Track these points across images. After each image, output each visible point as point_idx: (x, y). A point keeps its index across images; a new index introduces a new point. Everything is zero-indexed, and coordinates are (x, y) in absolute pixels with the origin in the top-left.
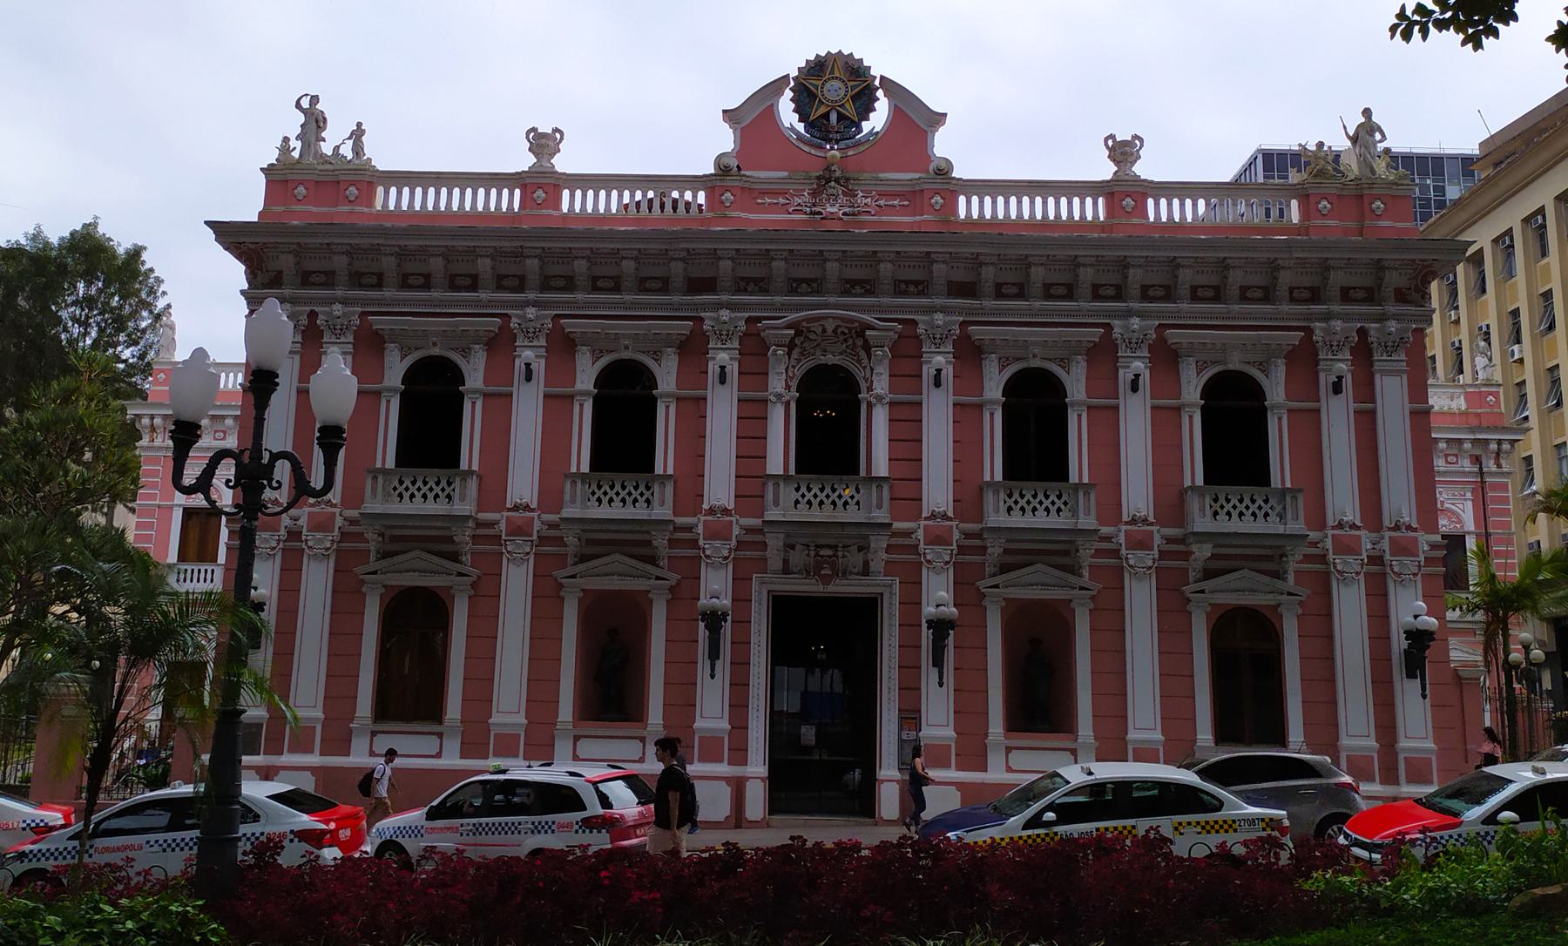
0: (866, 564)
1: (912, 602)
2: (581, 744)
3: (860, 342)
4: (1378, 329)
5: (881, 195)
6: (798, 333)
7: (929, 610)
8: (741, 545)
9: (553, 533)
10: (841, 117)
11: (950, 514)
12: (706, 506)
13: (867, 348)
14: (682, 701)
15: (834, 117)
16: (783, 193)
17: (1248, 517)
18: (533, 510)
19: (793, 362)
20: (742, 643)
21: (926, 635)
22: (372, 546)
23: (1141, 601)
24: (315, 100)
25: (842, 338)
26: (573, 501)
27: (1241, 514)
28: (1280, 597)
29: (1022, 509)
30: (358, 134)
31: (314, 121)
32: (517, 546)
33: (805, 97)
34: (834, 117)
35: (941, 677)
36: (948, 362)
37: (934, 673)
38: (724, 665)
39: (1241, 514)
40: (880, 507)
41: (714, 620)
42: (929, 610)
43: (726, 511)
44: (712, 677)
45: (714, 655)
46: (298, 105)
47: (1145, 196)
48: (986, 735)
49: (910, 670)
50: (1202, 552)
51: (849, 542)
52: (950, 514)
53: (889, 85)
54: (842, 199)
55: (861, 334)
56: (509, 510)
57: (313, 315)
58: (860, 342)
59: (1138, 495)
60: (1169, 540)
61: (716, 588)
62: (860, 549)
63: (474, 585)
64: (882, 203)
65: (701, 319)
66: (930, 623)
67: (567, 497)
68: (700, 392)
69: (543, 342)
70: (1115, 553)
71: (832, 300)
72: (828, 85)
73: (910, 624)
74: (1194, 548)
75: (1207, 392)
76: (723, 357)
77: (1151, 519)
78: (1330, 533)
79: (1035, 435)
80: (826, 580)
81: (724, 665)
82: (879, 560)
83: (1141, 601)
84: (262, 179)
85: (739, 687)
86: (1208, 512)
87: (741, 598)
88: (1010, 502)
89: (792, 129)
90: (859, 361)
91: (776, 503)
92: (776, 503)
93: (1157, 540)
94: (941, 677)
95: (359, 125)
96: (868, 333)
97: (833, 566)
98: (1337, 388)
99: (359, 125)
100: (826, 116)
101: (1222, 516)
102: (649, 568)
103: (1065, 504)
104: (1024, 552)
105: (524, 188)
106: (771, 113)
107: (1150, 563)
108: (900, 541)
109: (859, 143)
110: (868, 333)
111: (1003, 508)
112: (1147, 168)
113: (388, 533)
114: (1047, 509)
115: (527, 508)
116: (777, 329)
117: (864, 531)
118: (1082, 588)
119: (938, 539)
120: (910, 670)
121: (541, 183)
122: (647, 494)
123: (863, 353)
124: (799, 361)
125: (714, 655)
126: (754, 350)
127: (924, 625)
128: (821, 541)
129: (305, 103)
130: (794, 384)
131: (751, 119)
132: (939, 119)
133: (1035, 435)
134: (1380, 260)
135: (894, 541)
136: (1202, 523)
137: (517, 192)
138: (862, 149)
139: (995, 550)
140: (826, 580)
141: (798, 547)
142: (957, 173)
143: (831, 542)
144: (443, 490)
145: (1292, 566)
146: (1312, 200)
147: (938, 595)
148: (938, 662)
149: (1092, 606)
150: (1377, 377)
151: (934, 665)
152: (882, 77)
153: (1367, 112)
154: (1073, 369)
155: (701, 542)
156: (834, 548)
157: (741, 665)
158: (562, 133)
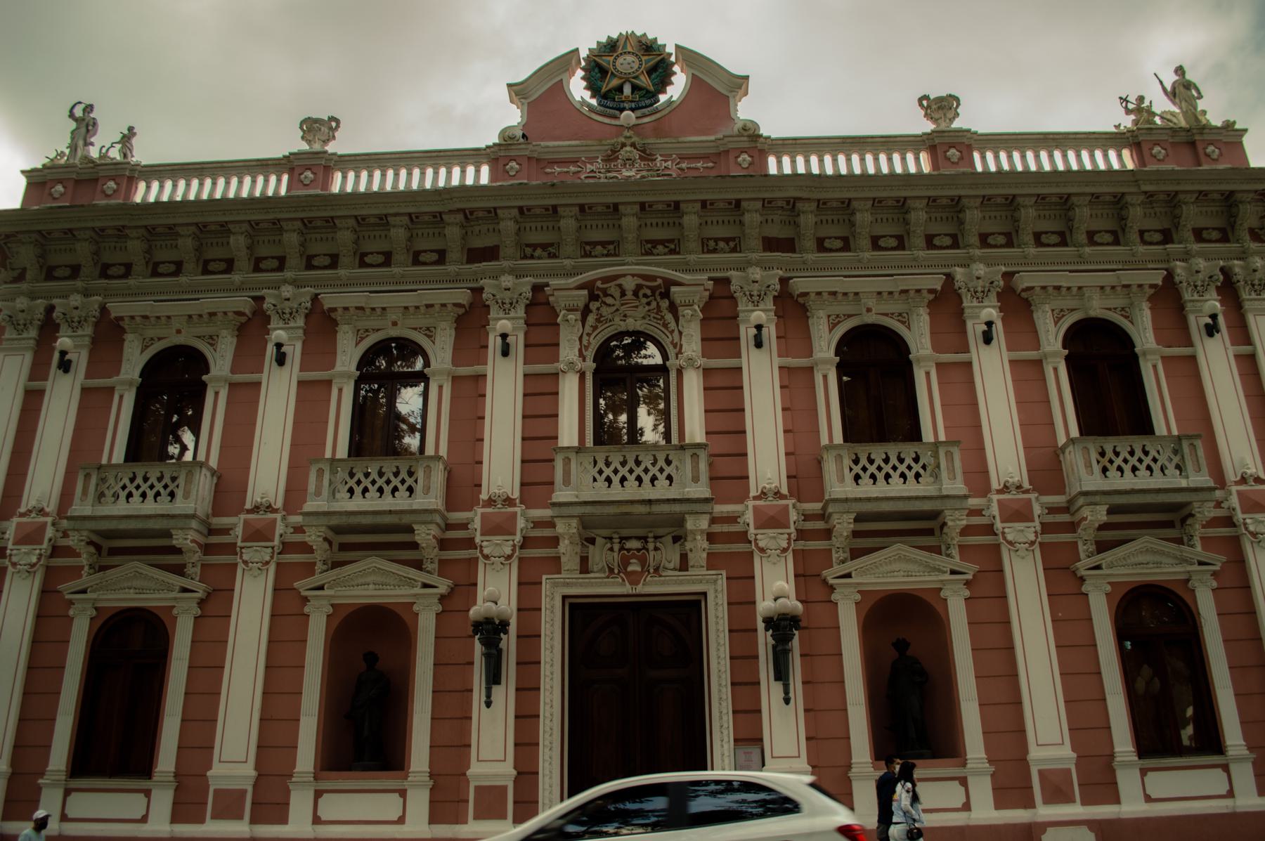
0: (684, 557)
1: (742, 601)
2: (325, 800)
3: (665, 304)
4: (1242, 267)
5: (683, 158)
6: (593, 297)
7: (765, 606)
8: (527, 542)
9: (298, 538)
10: (635, 88)
11: (785, 491)
12: (484, 496)
13: (673, 308)
14: (453, 744)
15: (627, 90)
16: (574, 162)
17: (1143, 472)
18: (276, 511)
19: (588, 329)
20: (529, 663)
21: (764, 639)
22: (84, 560)
23: (1026, 584)
24: (89, 108)
25: (644, 300)
26: (318, 493)
27: (1134, 469)
28: (1190, 568)
29: (873, 477)
30: (127, 138)
31: (85, 124)
32: (256, 553)
33: (597, 70)
34: (627, 90)
35: (786, 692)
36: (769, 320)
37: (777, 688)
38: (505, 695)
39: (1134, 469)
40: (696, 479)
41: (491, 630)
42: (765, 606)
43: (509, 501)
44: (488, 704)
45: (494, 677)
46: (72, 115)
47: (970, 149)
48: (849, 767)
49: (745, 686)
50: (1099, 514)
51: (660, 531)
52: (785, 491)
53: (689, 57)
54: (640, 164)
55: (666, 295)
56: (249, 512)
57: (50, 309)
58: (665, 304)
59: (1006, 456)
60: (1052, 510)
61: (496, 591)
62: (676, 539)
63: (202, 603)
64: (684, 165)
65: (481, 289)
66: (769, 622)
67: (312, 487)
68: (477, 369)
69: (300, 322)
70: (989, 529)
71: (630, 259)
72: (620, 60)
73: (741, 631)
74: (1086, 512)
75: (1068, 340)
76: (506, 322)
77: (1026, 485)
78: (1234, 489)
79: (877, 386)
80: (634, 579)
81: (505, 695)
82: (699, 548)
83: (1026, 584)
84: (23, 182)
85: (526, 717)
86: (1097, 469)
87: (529, 609)
88: (857, 469)
89: (583, 102)
90: (666, 325)
91: (567, 482)
92: (567, 482)
93: (1037, 510)
94: (786, 692)
95: (131, 129)
96: (674, 289)
97: (643, 562)
98: (1211, 330)
99: (131, 129)
100: (620, 89)
101: (1113, 472)
102: (412, 573)
103: (924, 467)
104: (879, 528)
105: (291, 171)
106: (559, 90)
107: (1032, 537)
108: (726, 528)
109: (657, 111)
110: (674, 289)
111: (849, 477)
112: (971, 119)
113: (106, 544)
114: (903, 475)
115: (270, 508)
116: (566, 291)
117: (677, 508)
118: (953, 572)
119: (772, 521)
120: (745, 686)
121: (309, 165)
122: (410, 481)
123: (669, 317)
124: (595, 328)
125: (494, 677)
126: (541, 315)
127: (761, 626)
128: (625, 533)
129: (78, 112)
130: (590, 354)
131: (539, 93)
132: (740, 84)
133: (877, 386)
134: (1232, 193)
135: (717, 528)
136: (1092, 481)
137: (285, 178)
138: (658, 116)
139: (843, 524)
140: (634, 579)
141: (599, 541)
142: (764, 131)
143: (641, 532)
144: (166, 487)
145: (1198, 531)
146: (1145, 147)
147: (776, 587)
148: (781, 674)
149: (967, 593)
150: (1251, 319)
151: (777, 678)
152: (677, 47)
153: (1180, 70)
154: (914, 326)
155: (478, 540)
156: (644, 539)
157: (528, 690)
158: (338, 121)
